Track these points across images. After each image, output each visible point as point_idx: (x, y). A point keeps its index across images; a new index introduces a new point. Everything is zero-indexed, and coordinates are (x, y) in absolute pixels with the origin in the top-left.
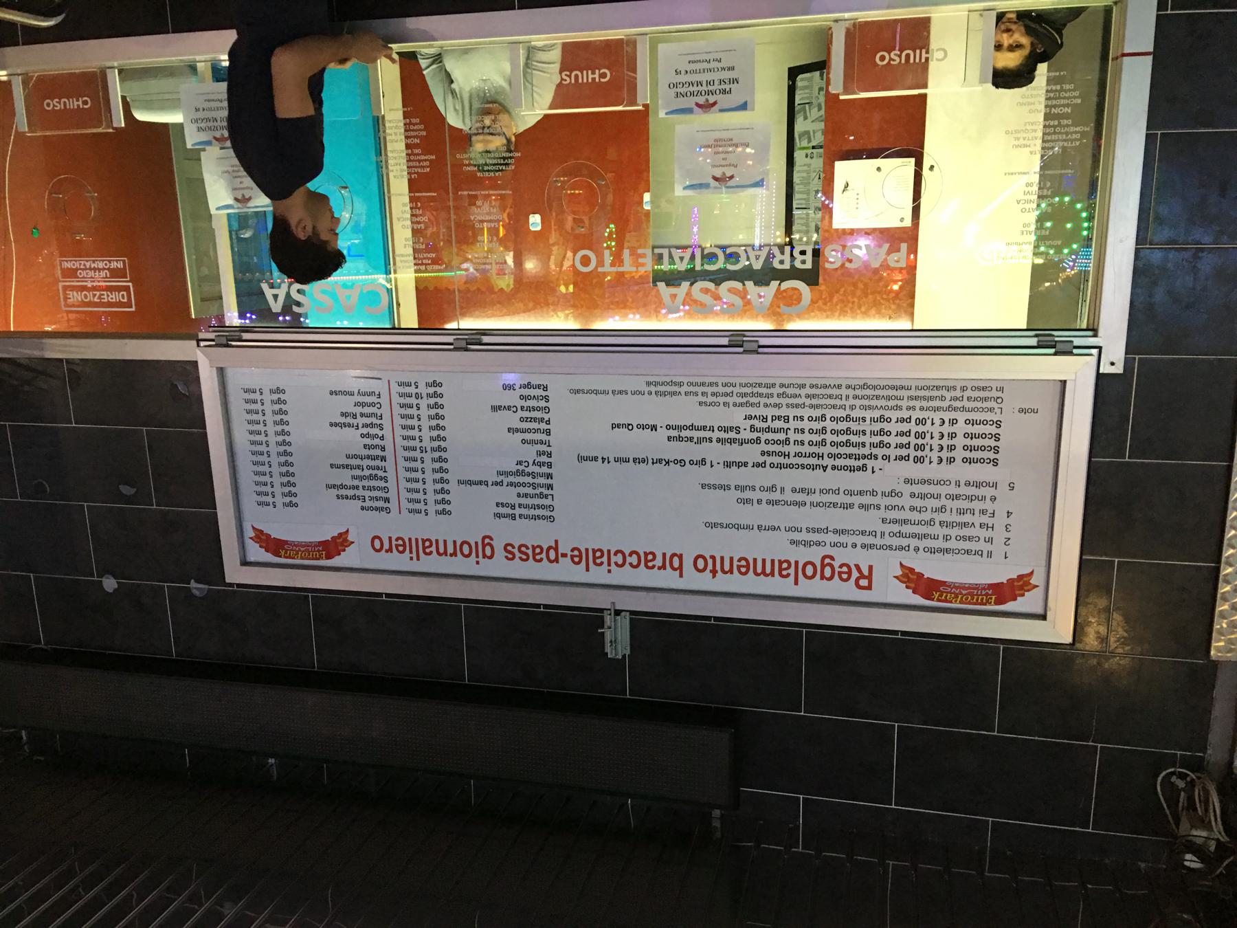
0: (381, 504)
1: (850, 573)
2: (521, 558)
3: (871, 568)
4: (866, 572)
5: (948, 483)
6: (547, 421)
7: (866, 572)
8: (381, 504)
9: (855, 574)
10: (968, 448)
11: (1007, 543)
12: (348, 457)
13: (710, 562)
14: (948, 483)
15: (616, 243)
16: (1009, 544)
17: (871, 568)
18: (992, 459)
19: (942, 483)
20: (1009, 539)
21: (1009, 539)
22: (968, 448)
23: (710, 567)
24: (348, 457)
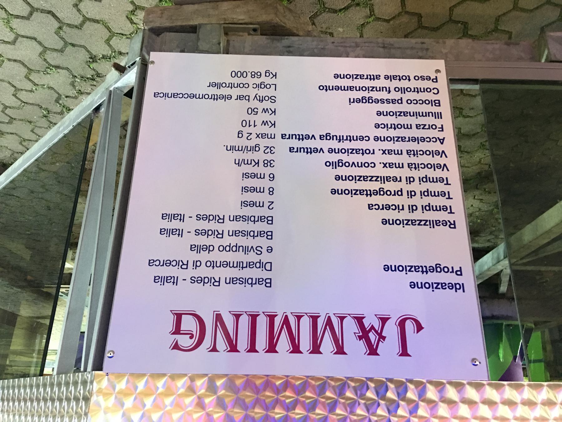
0: (256, 273)
1: (446, 223)
2: (239, 283)
3: (454, 221)
4: (453, 223)
5: (247, 86)
6: (457, 271)
7: (453, 223)
8: (256, 273)
9: (449, 224)
10: (406, 78)
11: (271, 207)
12: (337, 76)
13: (212, 263)
14: (247, 86)
15: (479, 223)
16: (273, 208)
17: (454, 221)
18: (424, 151)
19: (241, 85)
20: (273, 202)
21: (273, 202)
22: (406, 78)
23: (212, 265)
24: (337, 76)
